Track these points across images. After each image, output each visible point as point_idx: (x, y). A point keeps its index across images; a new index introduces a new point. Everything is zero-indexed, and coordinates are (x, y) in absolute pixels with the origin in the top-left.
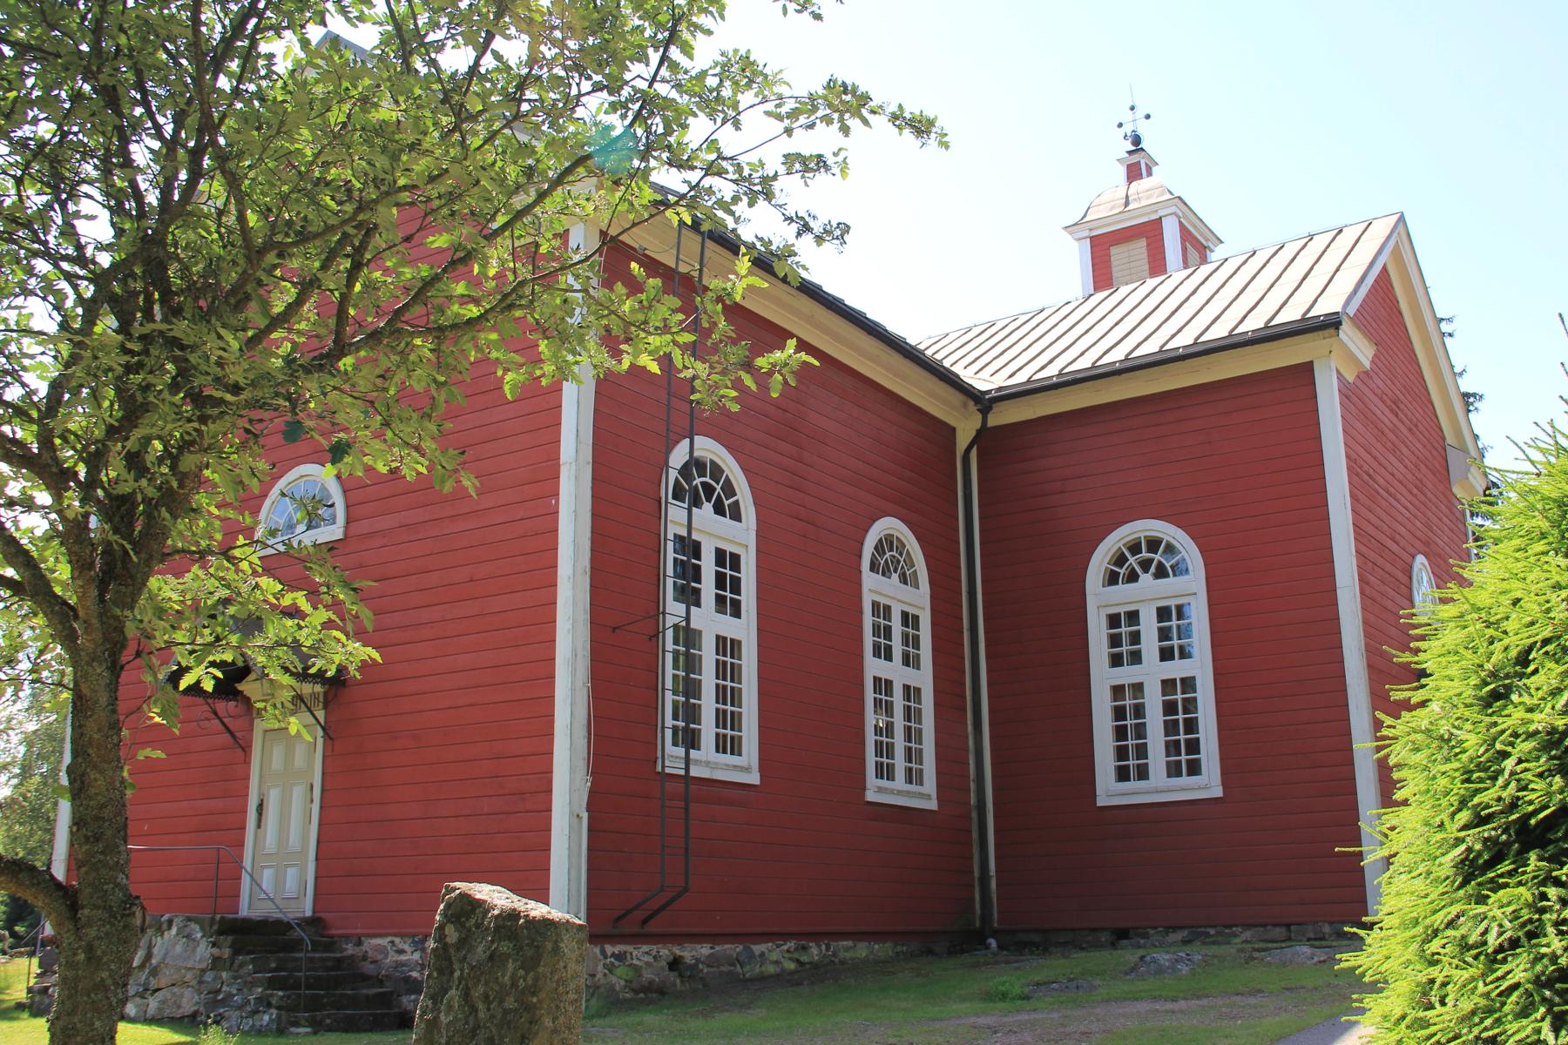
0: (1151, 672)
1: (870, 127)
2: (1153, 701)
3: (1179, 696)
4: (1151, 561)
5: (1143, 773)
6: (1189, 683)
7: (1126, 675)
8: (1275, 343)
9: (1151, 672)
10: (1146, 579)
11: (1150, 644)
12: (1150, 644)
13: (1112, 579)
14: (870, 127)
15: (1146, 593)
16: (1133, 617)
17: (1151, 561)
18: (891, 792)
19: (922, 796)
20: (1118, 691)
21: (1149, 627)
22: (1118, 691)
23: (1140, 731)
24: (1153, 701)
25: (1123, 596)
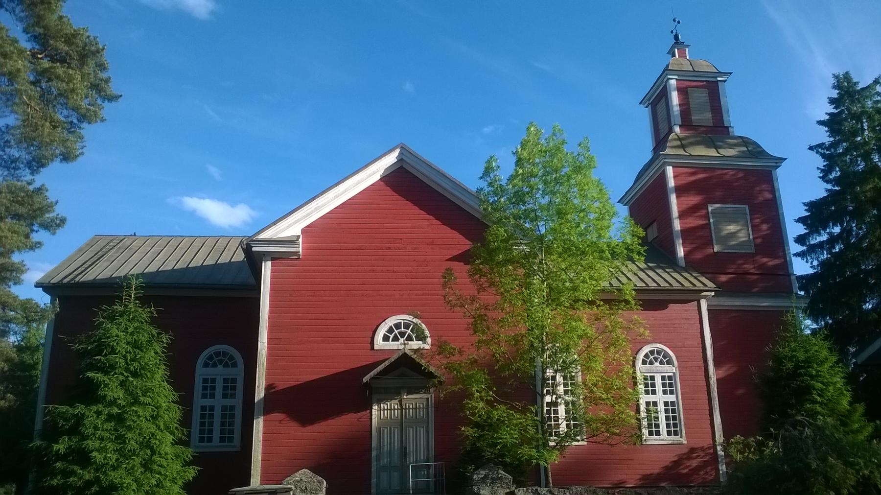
0: (660, 398)
1: (786, 159)
2: (218, 413)
3: (670, 408)
4: (215, 363)
5: (210, 440)
6: (232, 408)
7: (651, 398)
8: (703, 316)
9: (218, 402)
10: (220, 367)
11: (219, 391)
12: (219, 391)
13: (206, 365)
14: (786, 159)
15: (219, 372)
16: (214, 381)
17: (215, 363)
18: (662, 440)
19: (234, 446)
20: (203, 408)
21: (219, 385)
22: (203, 408)
23: (211, 424)
24: (218, 413)
25: (210, 372)
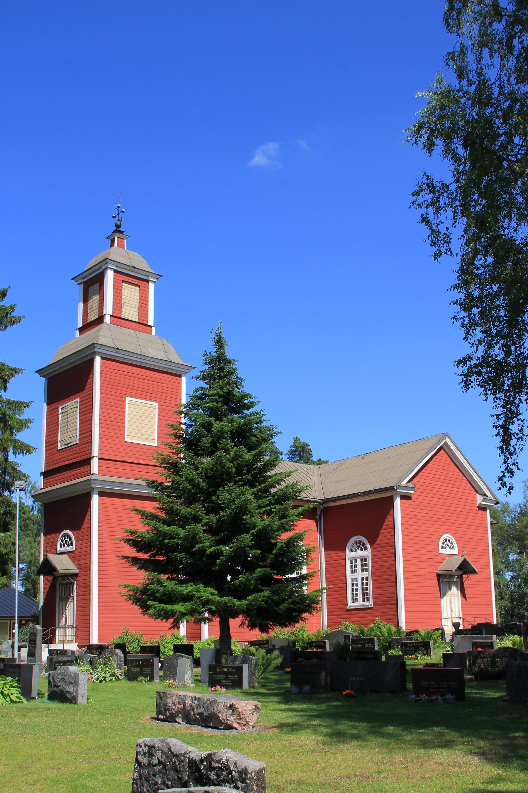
15: (359, 553)
